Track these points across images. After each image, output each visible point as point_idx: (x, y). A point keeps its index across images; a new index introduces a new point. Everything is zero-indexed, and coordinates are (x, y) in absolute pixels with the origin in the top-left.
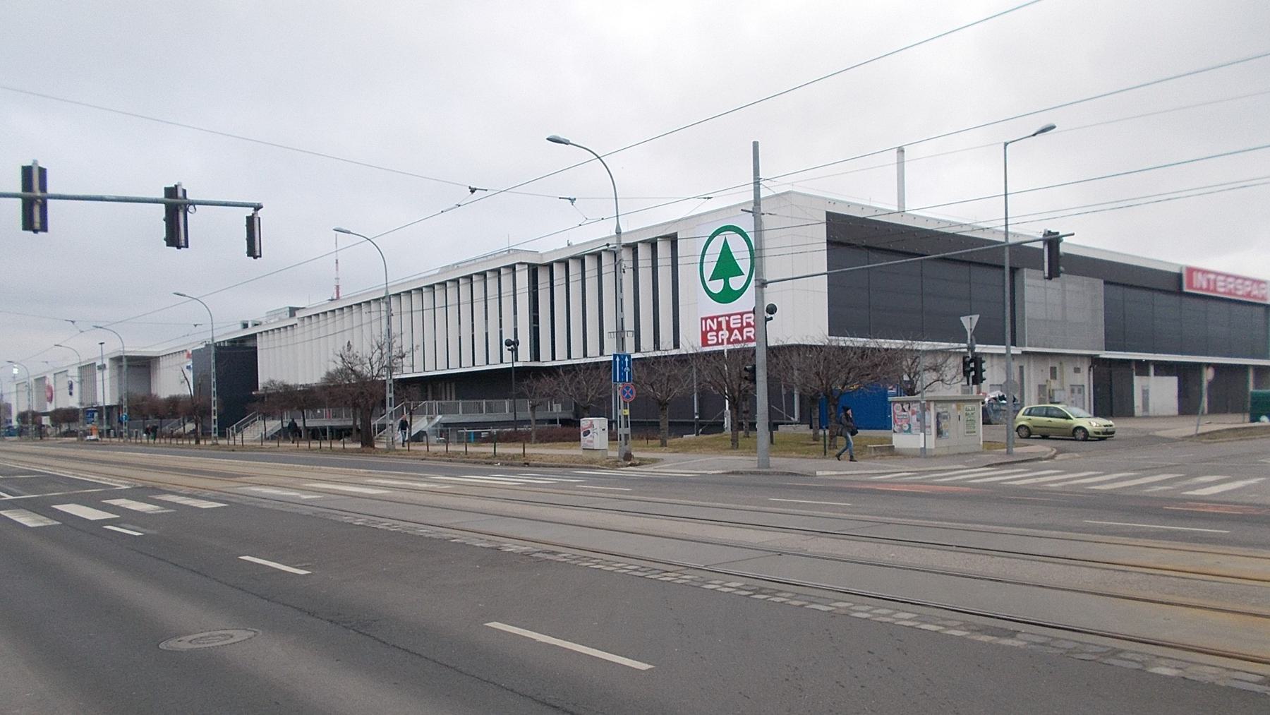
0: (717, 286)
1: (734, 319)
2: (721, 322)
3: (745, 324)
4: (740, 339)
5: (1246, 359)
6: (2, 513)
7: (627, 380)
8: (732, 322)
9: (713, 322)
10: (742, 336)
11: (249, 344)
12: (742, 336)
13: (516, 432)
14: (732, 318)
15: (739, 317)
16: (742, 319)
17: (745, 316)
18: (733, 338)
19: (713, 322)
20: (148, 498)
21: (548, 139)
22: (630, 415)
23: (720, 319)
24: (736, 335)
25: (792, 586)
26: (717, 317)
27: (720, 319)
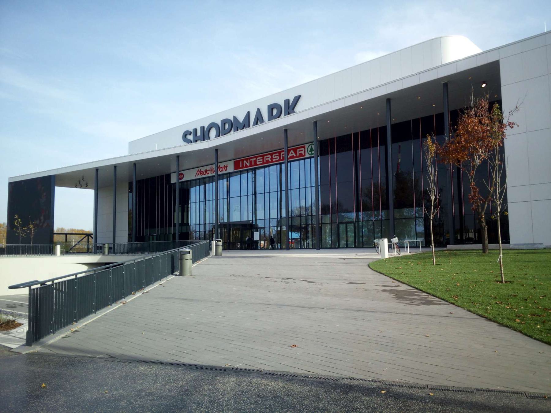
0: (310, 153)
1: (258, 159)
2: (252, 161)
4: (295, 155)
5: (388, 136)
7: (289, 160)
8: (257, 161)
9: (245, 163)
11: (136, 244)
12: (296, 153)
13: (254, 181)
14: (265, 157)
15: (262, 158)
16: (263, 159)
17: (282, 153)
23: (251, 160)
24: (292, 153)
25: (208, 209)
26: (250, 159)
27: (251, 160)
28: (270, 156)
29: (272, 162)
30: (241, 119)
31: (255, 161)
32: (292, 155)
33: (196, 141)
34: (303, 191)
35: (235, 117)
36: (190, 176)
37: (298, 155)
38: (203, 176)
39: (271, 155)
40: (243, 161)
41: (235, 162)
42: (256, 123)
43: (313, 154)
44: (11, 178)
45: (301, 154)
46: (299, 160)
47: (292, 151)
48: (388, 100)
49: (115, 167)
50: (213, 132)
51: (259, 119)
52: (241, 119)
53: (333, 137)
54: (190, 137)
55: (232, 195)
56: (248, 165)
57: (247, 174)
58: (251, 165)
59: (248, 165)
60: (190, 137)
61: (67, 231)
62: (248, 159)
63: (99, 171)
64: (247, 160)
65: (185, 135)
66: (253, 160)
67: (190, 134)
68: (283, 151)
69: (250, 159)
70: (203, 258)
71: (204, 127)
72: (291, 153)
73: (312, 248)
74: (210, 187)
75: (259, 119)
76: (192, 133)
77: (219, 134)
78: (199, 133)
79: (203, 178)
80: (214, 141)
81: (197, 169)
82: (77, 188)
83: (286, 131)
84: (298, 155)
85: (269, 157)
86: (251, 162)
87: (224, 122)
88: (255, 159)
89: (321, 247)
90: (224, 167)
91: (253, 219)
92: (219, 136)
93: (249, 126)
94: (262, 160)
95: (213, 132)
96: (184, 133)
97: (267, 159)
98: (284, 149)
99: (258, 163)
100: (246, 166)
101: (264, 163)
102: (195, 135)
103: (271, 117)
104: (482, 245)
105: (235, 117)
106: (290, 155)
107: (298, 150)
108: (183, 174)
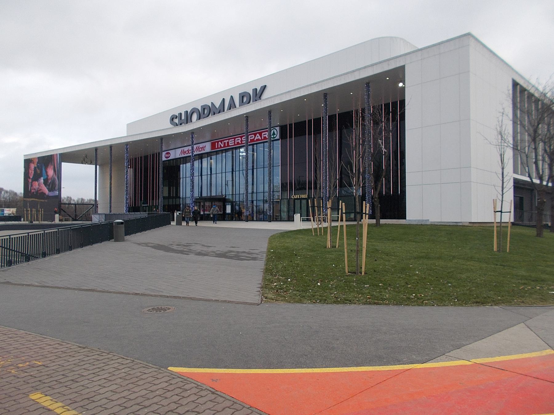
2: (225, 142)
3: (236, 143)
4: (260, 139)
6: (552, 352)
8: (230, 142)
9: (220, 145)
10: (261, 137)
12: (261, 137)
13: (518, 133)
15: (233, 140)
16: (235, 141)
18: (256, 138)
19: (220, 145)
20: (499, 251)
21: (224, 99)
22: (32, 225)
23: (225, 141)
24: (258, 137)
27: (225, 141)
28: (240, 138)
29: (242, 143)
30: (217, 105)
31: (228, 143)
32: (258, 138)
33: (181, 124)
34: (184, 176)
35: (212, 103)
36: (176, 154)
37: (263, 138)
38: (186, 155)
39: (241, 137)
40: (218, 142)
41: (212, 143)
42: (230, 108)
43: (244, 143)
44: (26, 155)
45: (239, 142)
46: (264, 142)
47: (258, 135)
48: (325, 94)
49: (111, 147)
50: (195, 117)
51: (232, 105)
52: (217, 105)
53: (388, 102)
54: (176, 121)
55: (203, 174)
56: (222, 146)
57: (215, 156)
58: (224, 146)
59: (222, 146)
60: (176, 121)
61: (86, 201)
62: (222, 141)
63: (98, 151)
64: (221, 142)
65: (172, 119)
66: (226, 141)
67: (176, 118)
68: (244, 136)
69: (224, 140)
70: (163, 226)
71: (187, 111)
72: (257, 136)
73: (257, 221)
74: (197, 164)
75: (232, 105)
76: (178, 118)
77: (199, 118)
78: (183, 118)
79: (186, 157)
80: (196, 124)
81: (181, 149)
82: (82, 164)
83: (270, 112)
84: (263, 138)
85: (239, 140)
86: (225, 143)
87: (204, 108)
88: (228, 141)
89: (272, 220)
90: (203, 148)
91: (256, 194)
92: (199, 119)
93: (224, 111)
94: (233, 142)
95: (195, 117)
96: (192, 109)
97: (264, 136)
98: (267, 129)
99: (230, 145)
100: (221, 147)
101: (235, 145)
102: (241, 102)
103: (242, 103)
104: (375, 220)
105: (212, 103)
106: (256, 138)
107: (263, 134)
108: (170, 153)
